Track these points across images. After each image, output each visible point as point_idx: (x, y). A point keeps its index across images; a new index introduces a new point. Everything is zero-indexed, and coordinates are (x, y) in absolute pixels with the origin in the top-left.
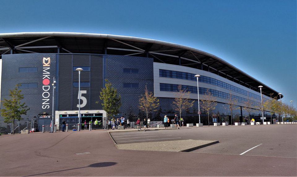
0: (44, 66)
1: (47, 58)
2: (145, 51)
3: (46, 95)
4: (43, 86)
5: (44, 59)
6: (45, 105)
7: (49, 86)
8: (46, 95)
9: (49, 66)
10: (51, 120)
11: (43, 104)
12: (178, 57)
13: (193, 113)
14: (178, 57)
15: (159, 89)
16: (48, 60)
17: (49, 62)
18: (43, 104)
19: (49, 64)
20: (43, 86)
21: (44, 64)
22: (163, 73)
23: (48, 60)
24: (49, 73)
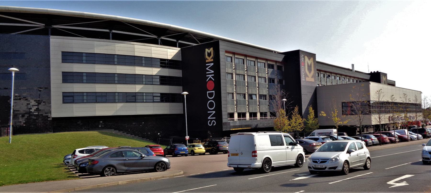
0: (207, 61)
1: (209, 49)
2: (44, 25)
3: (211, 105)
4: (208, 92)
5: (207, 50)
6: (212, 120)
7: (214, 92)
8: (211, 105)
9: (212, 60)
10: (14, 109)
11: (209, 118)
12: (175, 41)
13: (349, 167)
14: (175, 41)
15: (61, 81)
16: (211, 52)
17: (212, 56)
18: (209, 118)
19: (212, 58)
20: (208, 92)
21: (207, 59)
22: (68, 57)
23: (211, 52)
24: (213, 72)
